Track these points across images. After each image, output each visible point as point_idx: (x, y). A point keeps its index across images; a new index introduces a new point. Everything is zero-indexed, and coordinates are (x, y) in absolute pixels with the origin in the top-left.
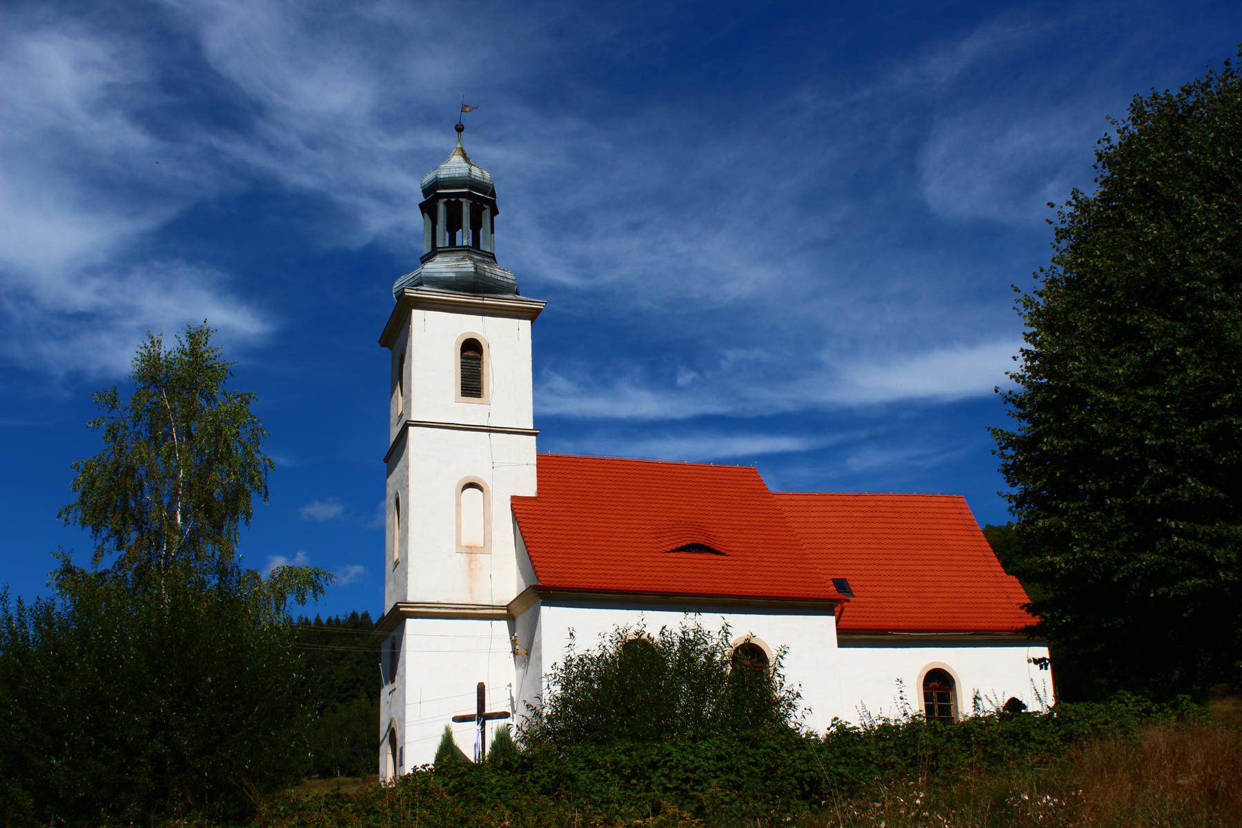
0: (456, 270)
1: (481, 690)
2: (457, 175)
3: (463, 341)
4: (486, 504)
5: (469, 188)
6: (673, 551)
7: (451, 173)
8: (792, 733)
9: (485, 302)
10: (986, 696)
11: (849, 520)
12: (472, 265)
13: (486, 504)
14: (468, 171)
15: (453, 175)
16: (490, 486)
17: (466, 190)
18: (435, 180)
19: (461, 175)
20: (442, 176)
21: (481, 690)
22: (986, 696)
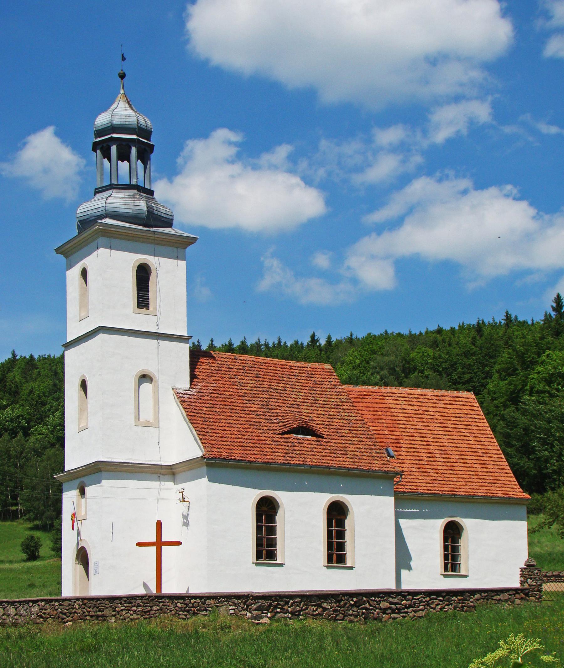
0: (132, 207)
1: (159, 524)
2: (127, 123)
3: (138, 265)
4: (156, 392)
5: (138, 136)
6: (283, 433)
7: (122, 120)
8: (328, 203)
9: (133, 202)
10: (73, 529)
11: (417, 484)
12: (145, 204)
13: (156, 392)
14: (136, 120)
15: (124, 123)
16: (156, 374)
17: (135, 137)
18: (109, 125)
19: (131, 123)
20: (115, 123)
21: (159, 524)
22: (73, 529)
